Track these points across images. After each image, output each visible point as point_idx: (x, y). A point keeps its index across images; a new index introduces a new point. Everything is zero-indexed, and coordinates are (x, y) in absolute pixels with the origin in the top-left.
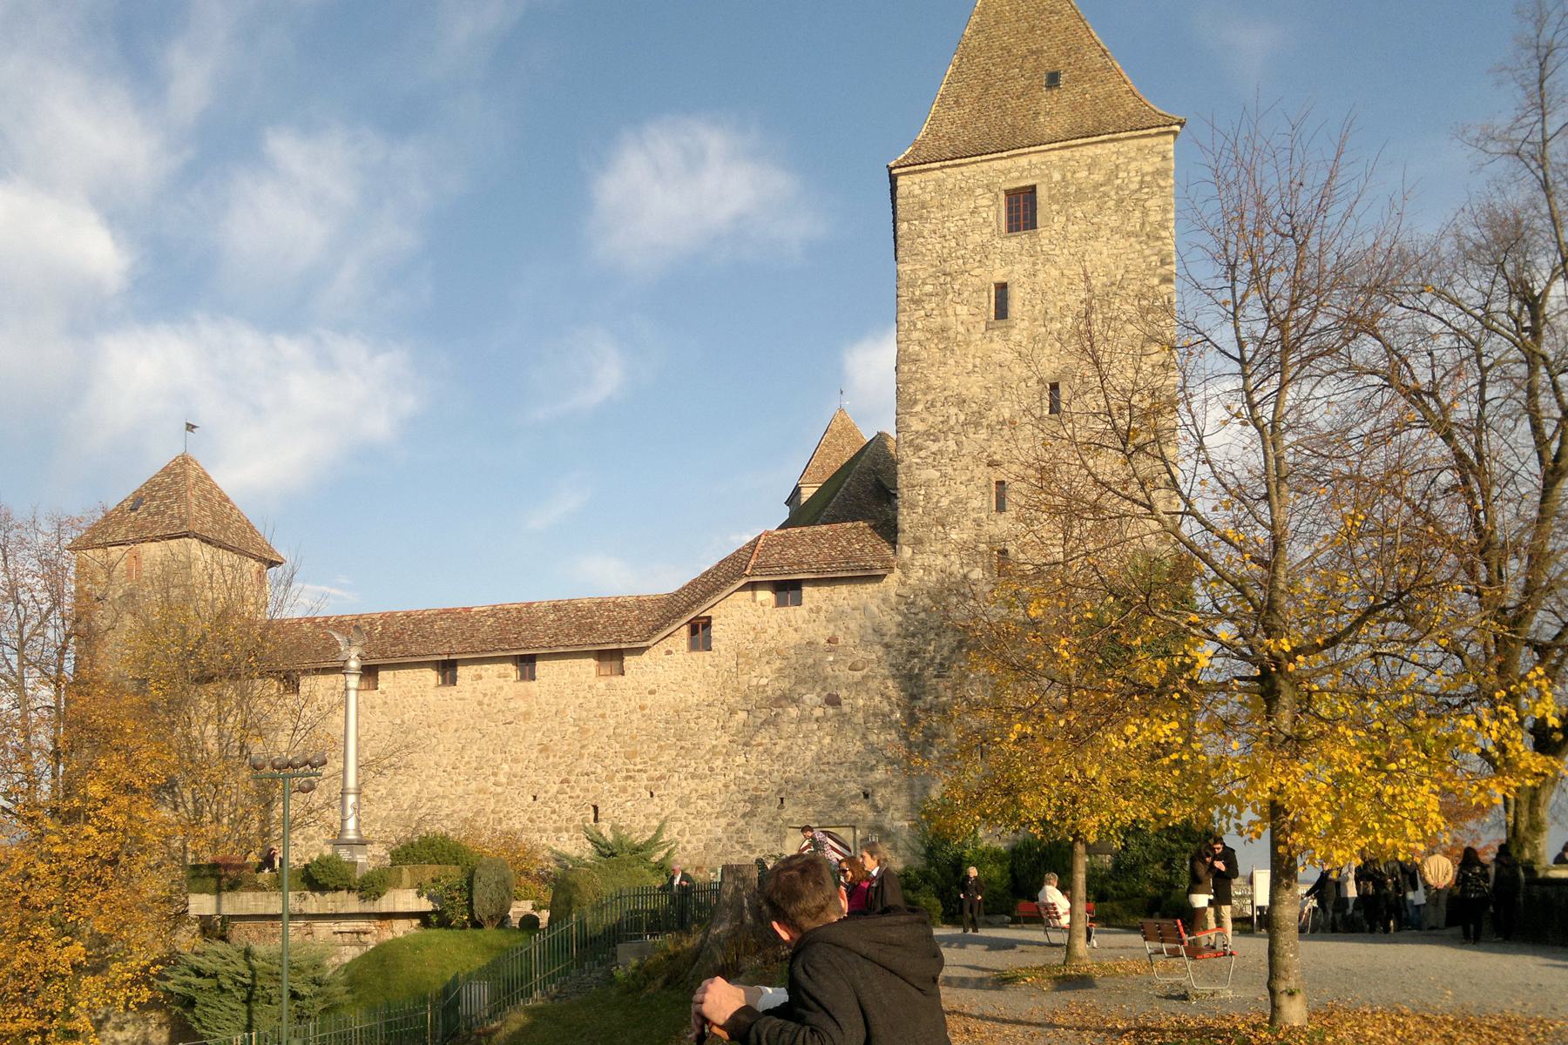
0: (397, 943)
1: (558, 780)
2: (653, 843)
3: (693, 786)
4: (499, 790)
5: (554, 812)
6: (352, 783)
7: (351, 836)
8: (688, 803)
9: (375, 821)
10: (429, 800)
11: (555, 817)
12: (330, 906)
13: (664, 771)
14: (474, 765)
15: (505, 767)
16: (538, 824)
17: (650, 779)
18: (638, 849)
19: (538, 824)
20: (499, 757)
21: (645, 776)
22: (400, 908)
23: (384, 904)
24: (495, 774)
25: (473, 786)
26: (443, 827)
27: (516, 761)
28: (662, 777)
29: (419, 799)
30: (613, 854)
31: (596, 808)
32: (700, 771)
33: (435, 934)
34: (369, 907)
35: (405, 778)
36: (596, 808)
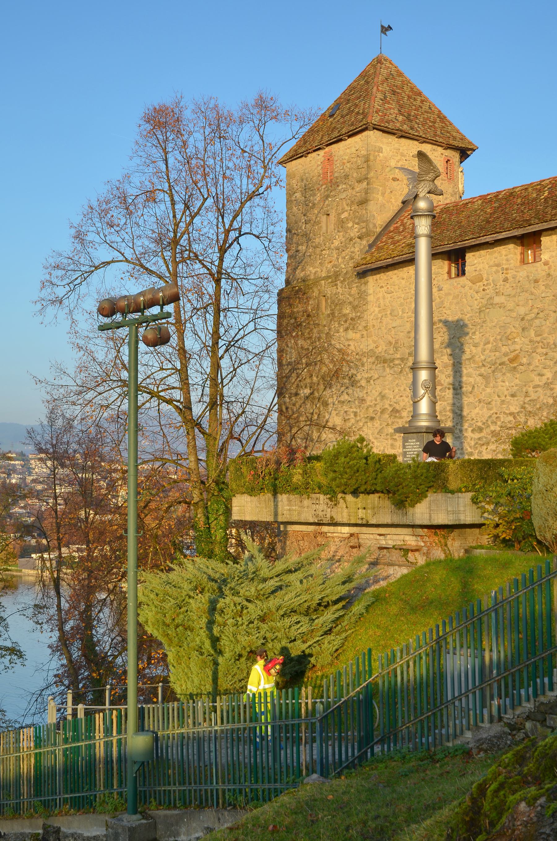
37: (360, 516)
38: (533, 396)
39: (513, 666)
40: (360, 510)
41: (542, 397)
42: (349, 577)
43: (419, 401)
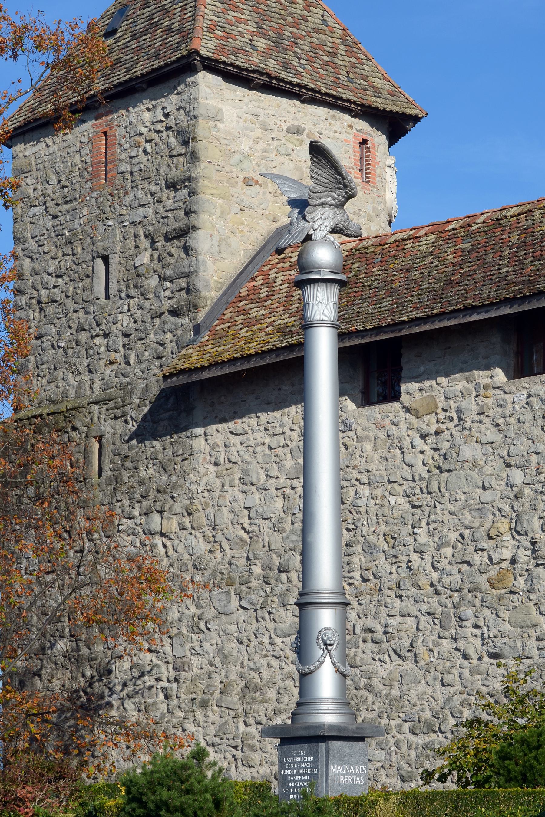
7: (328, 717)
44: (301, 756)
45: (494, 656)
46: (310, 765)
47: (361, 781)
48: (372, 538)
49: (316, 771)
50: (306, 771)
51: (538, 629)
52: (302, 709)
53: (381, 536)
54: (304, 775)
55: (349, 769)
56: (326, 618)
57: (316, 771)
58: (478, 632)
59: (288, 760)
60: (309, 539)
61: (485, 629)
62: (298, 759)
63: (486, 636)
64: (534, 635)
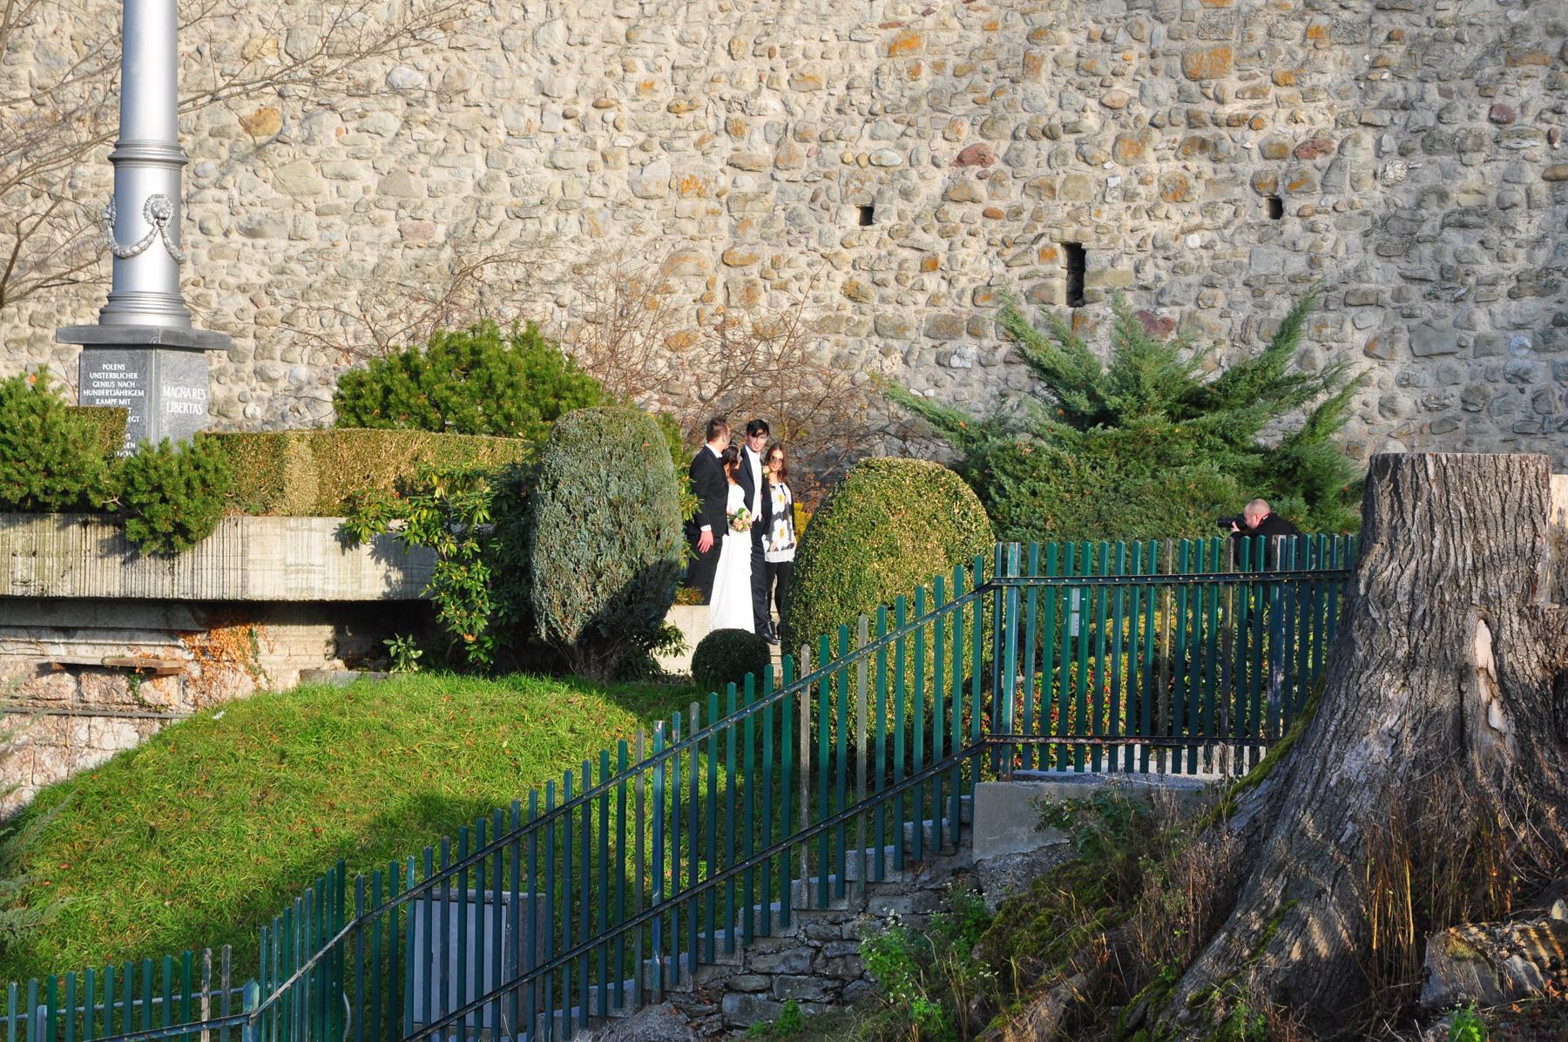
0: (265, 719)
1: (947, 151)
2: (1259, 383)
3: (1430, 177)
4: (749, 183)
5: (930, 265)
6: (152, 122)
7: (152, 317)
8: (1411, 241)
9: (341, 279)
10: (519, 214)
11: (932, 282)
12: (22, 568)
13: (1324, 122)
14: (666, 95)
15: (770, 103)
16: (876, 307)
17: (1273, 152)
18: (1195, 401)
19: (876, 307)
20: (749, 71)
21: (1253, 140)
22: (266, 586)
23: (204, 573)
24: (732, 130)
25: (662, 168)
26: (560, 315)
27: (801, 81)
28: (1314, 146)
29: (482, 212)
30: (1108, 417)
31: (1076, 254)
32: (1458, 123)
33: (410, 689)
34: (151, 579)
35: (435, 137)
36: (1076, 254)
37: (18, 576)
38: (316, 239)
39: (156, 989)
40: (19, 559)
41: (344, 245)
42: (619, 678)
43: (135, 254)
44: (119, 372)
45: (251, 233)
46: (133, 384)
47: (199, 410)
48: (53, 42)
49: (141, 393)
50: (125, 393)
51: (320, 198)
52: (117, 306)
53: (67, 40)
54: (122, 397)
55: (185, 392)
56: (151, 182)
57: (141, 393)
58: (223, 195)
59: (95, 375)
60: (134, 70)
61: (235, 193)
62: (115, 376)
63: (236, 202)
64: (313, 207)
